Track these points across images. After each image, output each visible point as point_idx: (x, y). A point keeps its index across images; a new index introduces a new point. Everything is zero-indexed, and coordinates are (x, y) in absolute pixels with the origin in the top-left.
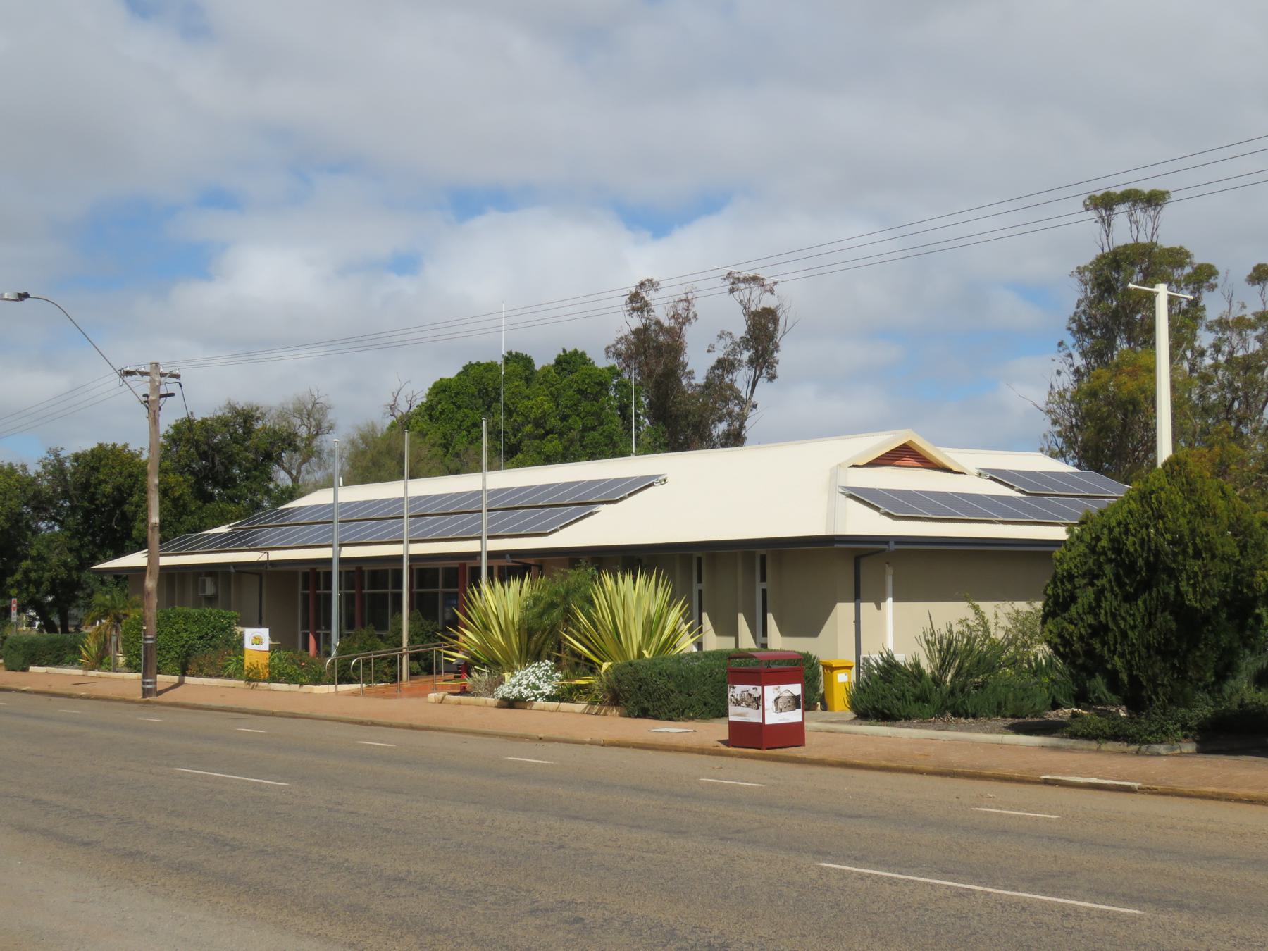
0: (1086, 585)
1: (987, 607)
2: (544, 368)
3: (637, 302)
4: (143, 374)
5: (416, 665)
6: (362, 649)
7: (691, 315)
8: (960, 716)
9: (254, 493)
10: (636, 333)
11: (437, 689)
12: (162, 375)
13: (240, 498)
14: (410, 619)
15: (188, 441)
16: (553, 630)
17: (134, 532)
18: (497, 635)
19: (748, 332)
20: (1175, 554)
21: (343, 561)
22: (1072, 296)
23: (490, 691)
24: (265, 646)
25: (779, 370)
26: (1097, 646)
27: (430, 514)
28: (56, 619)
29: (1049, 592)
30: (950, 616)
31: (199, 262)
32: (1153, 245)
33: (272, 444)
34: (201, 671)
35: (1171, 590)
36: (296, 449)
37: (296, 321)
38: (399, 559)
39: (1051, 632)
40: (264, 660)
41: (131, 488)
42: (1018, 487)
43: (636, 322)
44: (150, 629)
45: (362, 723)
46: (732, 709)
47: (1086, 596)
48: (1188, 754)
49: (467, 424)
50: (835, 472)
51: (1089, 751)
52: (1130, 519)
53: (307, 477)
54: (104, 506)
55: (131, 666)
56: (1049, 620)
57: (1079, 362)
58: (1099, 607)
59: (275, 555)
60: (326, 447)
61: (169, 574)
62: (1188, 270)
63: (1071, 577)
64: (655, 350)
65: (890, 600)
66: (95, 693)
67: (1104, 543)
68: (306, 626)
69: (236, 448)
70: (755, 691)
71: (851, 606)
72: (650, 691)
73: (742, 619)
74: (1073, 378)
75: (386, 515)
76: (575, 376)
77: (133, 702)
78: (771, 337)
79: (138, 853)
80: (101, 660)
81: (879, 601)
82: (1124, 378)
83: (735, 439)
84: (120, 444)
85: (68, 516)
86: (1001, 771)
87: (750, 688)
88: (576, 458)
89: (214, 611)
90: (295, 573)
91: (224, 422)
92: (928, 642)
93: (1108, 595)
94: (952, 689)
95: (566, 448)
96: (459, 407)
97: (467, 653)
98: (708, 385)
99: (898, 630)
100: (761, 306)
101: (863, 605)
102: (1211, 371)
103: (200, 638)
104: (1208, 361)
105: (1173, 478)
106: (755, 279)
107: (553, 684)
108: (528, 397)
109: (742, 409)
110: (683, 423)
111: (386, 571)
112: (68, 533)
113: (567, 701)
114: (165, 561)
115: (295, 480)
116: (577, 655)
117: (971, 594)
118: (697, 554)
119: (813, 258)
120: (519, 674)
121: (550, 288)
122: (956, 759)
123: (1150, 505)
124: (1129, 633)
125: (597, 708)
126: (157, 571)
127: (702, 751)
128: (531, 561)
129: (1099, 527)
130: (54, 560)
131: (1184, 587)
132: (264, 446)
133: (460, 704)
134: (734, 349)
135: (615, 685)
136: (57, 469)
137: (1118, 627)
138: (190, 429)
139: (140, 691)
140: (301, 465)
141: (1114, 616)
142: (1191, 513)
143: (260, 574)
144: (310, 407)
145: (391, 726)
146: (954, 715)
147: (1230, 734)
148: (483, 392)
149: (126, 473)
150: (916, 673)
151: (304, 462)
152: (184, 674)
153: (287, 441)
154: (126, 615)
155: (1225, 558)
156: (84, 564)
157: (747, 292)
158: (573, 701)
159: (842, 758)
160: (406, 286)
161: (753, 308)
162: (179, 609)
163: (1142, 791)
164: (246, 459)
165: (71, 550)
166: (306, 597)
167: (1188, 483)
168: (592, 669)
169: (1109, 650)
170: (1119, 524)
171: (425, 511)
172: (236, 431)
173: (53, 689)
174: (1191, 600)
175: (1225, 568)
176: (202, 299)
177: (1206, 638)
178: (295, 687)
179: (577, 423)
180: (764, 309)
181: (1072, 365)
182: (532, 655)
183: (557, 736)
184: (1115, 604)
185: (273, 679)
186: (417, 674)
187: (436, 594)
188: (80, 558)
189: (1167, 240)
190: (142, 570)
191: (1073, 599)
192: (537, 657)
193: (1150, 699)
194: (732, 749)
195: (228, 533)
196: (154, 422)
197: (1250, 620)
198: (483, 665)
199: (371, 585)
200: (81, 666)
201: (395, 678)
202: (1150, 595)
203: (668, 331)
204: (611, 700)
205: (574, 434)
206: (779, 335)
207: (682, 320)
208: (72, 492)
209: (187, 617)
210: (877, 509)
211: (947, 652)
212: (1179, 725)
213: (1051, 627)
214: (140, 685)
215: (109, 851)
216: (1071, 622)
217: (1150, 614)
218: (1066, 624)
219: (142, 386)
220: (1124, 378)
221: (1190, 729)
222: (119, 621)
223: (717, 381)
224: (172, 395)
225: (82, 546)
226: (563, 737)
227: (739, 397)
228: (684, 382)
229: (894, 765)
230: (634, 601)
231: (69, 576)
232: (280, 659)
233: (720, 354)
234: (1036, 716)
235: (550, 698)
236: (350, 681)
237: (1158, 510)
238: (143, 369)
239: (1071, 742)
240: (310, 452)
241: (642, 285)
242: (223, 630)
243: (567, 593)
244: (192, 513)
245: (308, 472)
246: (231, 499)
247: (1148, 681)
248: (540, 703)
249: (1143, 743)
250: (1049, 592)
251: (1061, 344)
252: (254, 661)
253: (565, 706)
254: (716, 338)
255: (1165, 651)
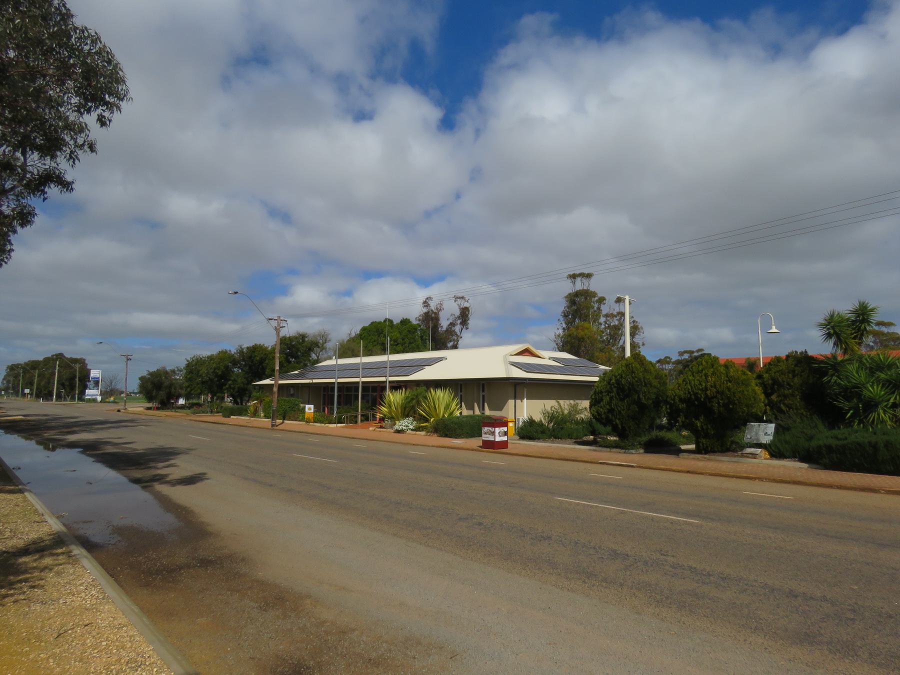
1: (561, 402)
3: (426, 304)
16: (413, 407)
23: (391, 427)
24: (312, 411)
28: (239, 400)
30: (550, 404)
31: (284, 291)
35: (636, 397)
38: (358, 383)
43: (425, 310)
44: (275, 405)
47: (606, 399)
50: (505, 357)
55: (266, 417)
57: (564, 326)
63: (601, 392)
64: (431, 318)
68: (324, 404)
72: (447, 428)
75: (354, 368)
80: (255, 414)
83: (455, 347)
91: (296, 338)
94: (556, 429)
99: (528, 409)
104: (603, 326)
106: (463, 298)
114: (280, 382)
116: (421, 415)
117: (557, 397)
119: (480, 294)
121: (397, 300)
122: (563, 454)
127: (472, 450)
131: (641, 396)
136: (241, 352)
150: (540, 424)
152: (284, 419)
153: (316, 344)
155: (655, 387)
156: (249, 383)
160: (348, 299)
168: (427, 421)
174: (644, 401)
176: (285, 302)
179: (407, 341)
182: (406, 415)
189: (592, 289)
190: (272, 385)
191: (602, 400)
192: (407, 416)
196: (278, 335)
199: (348, 392)
201: (356, 422)
203: (435, 313)
207: (439, 309)
211: (552, 417)
219: (275, 324)
230: (442, 397)
233: (451, 321)
240: (323, 348)
248: (409, 431)
253: (418, 433)
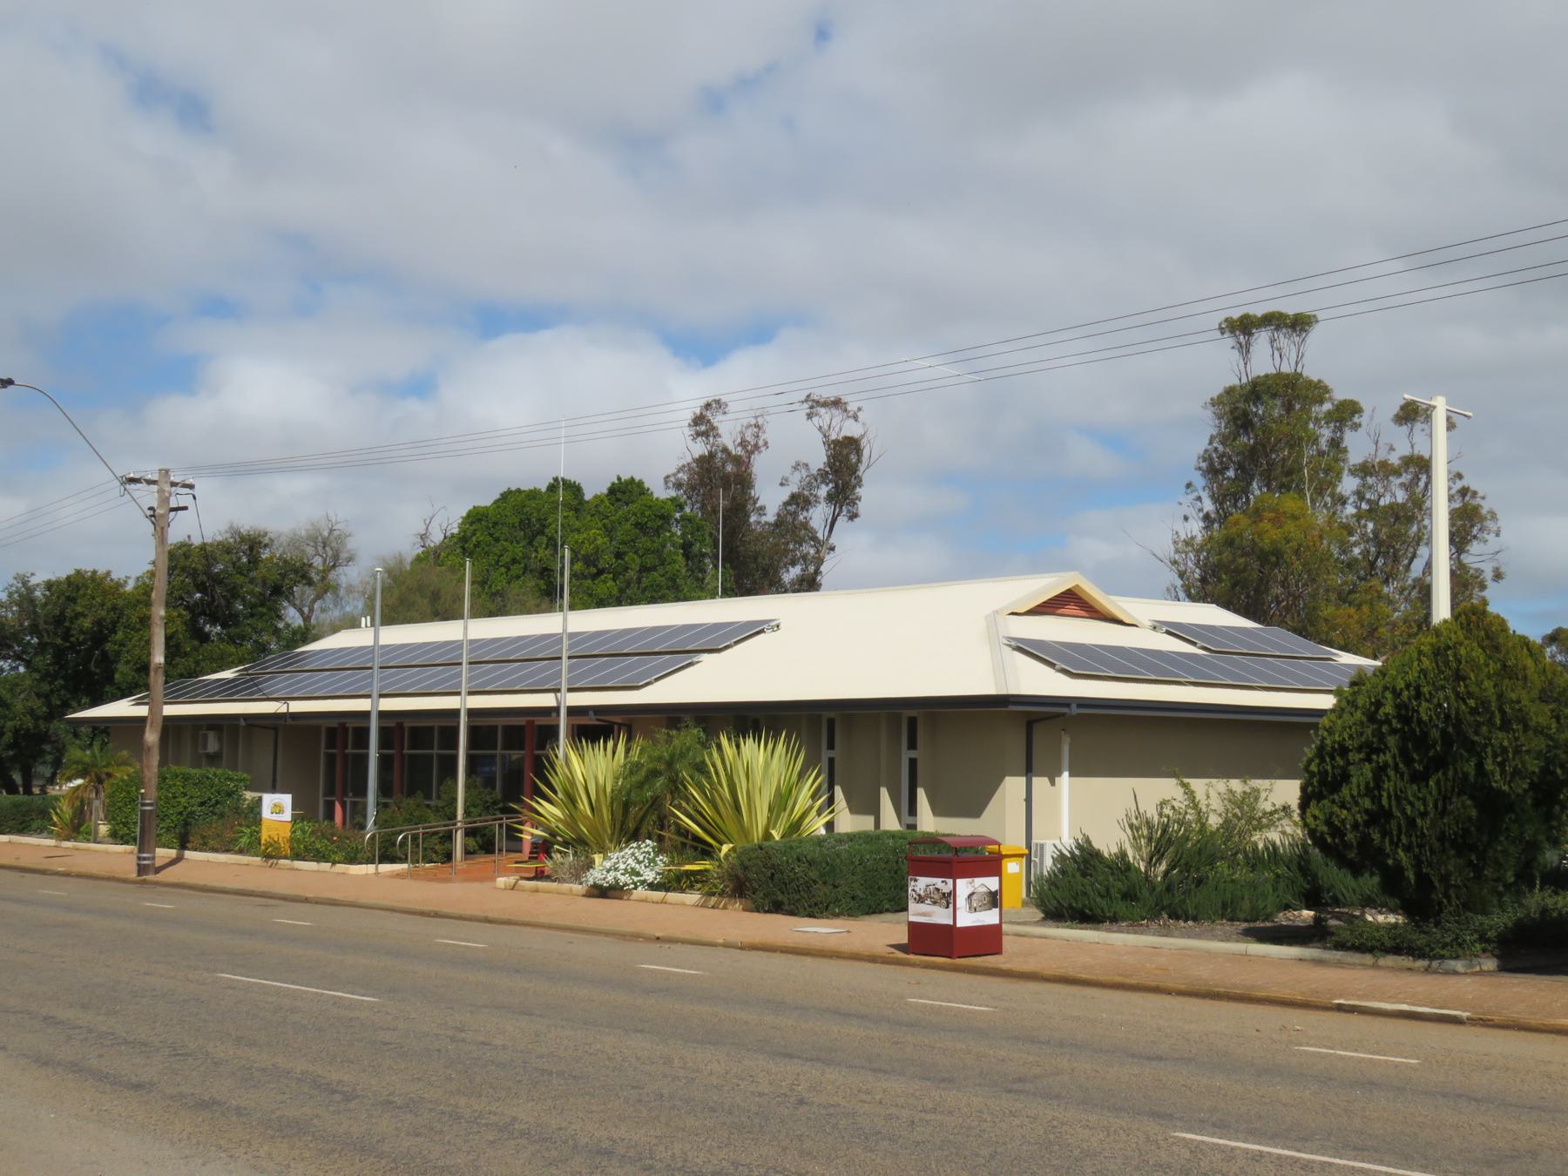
0: (1361, 760)
1: (1198, 785)
2: (596, 497)
3: (702, 424)
4: (150, 482)
5: (472, 842)
6: (408, 821)
7: (761, 443)
8: (1177, 918)
9: (259, 632)
10: (701, 460)
11: (506, 872)
12: (173, 484)
13: (243, 638)
14: (468, 787)
15: (183, 569)
16: (656, 803)
17: (117, 676)
18: (584, 806)
19: (829, 464)
20: (1479, 725)
21: (383, 715)
22: (1198, 433)
24: (287, 816)
25: (862, 507)
26: (1376, 836)
27: (496, 661)
29: (1314, 768)
30: (1155, 794)
32: (1298, 375)
33: (283, 576)
34: (205, 844)
35: (1470, 767)
36: (310, 583)
37: (294, 436)
38: (455, 713)
39: (1315, 818)
40: (286, 833)
41: (114, 623)
42: (1200, 643)
43: (700, 448)
44: (150, 793)
45: (422, 914)
46: (912, 906)
47: (1362, 774)
48: (1489, 973)
49: (506, 559)
50: (992, 619)
51: (1364, 966)
52: (1422, 681)
53: (322, 616)
54: (80, 644)
55: (116, 837)
56: (1313, 803)
57: (1208, 506)
58: (1379, 787)
59: (297, 707)
60: (343, 581)
61: (173, 726)
62: (1327, 406)
63: (1343, 750)
64: (720, 478)
65: (1066, 774)
66: (75, 869)
67: (1388, 709)
68: (330, 791)
69: (240, 580)
70: (944, 884)
71: (1021, 781)
72: (780, 880)
73: (884, 792)
74: (1201, 524)
76: (633, 507)
77: (125, 881)
78: (853, 470)
79: (215, 1102)
80: (77, 827)
81: (1053, 776)
82: (1266, 525)
83: (809, 583)
84: (101, 571)
85: (36, 654)
86: (1275, 992)
87: (938, 881)
88: (633, 601)
89: (219, 772)
90: (318, 728)
91: (226, 549)
92: (1131, 826)
93: (1391, 773)
94: (1178, 883)
95: (622, 591)
96: (497, 540)
97: (547, 829)
98: (779, 523)
99: (1076, 812)
100: (843, 434)
101: (1035, 779)
102: (1353, 522)
103: (202, 804)
104: (1350, 510)
105: (1470, 631)
106: (837, 403)
107: (657, 869)
108: (578, 530)
109: (818, 552)
110: (753, 566)
111: (431, 729)
112: (36, 676)
113: (674, 890)
114: (170, 710)
115: (307, 619)
117: (1182, 769)
118: (827, 715)
120: (615, 856)
123: (1447, 663)
124: (1419, 821)
125: (714, 900)
126: (160, 722)
127: (873, 959)
128: (617, 719)
129: (1380, 688)
130: (19, 707)
131: (1489, 765)
132: (274, 577)
133: (537, 891)
134: (810, 483)
135: (740, 873)
137: (1404, 812)
138: (186, 556)
139: (135, 868)
140: (314, 601)
141: (1398, 798)
142: (1497, 674)
143: (275, 729)
144: (326, 533)
145: (460, 918)
146: (1170, 917)
147: (1537, 948)
148: (525, 524)
149: (109, 605)
150: (1121, 866)
151: (318, 597)
154: (109, 775)
155: (1540, 731)
156: (56, 712)
157: (827, 418)
158: (682, 891)
159: (1061, 972)
161: (833, 437)
162: (174, 768)
163: (1472, 1022)
164: (251, 593)
165: (38, 695)
166: (331, 759)
167: (1488, 637)
168: (706, 852)
169: (1391, 841)
170: (1408, 686)
171: (491, 658)
172: (239, 559)
173: (23, 863)
174: (1498, 782)
175: (1540, 744)
177: (1507, 829)
178: (326, 866)
180: (846, 438)
181: (1201, 510)
182: (629, 833)
183: (679, 934)
184: (1400, 784)
185: (297, 856)
186: (474, 853)
187: (439, 756)
188: (49, 705)
189: (1311, 372)
190: (141, 720)
191: (1345, 777)
192: (635, 836)
193: (1440, 903)
194: (912, 957)
195: (234, 680)
197: (1557, 808)
198: (566, 844)
199: (417, 747)
200: (51, 834)
201: (448, 857)
202: (1445, 774)
203: (737, 460)
204: (734, 891)
205: (631, 574)
206: (862, 467)
207: (751, 448)
208: (42, 626)
209: (186, 778)
210: (1052, 665)
211: (1161, 840)
212: (1476, 936)
213: (1317, 813)
214: (133, 859)
215: (172, 1097)
216: (1343, 806)
217: (1445, 798)
218: (1336, 809)
219: (147, 496)
220: (1266, 525)
221: (1488, 941)
222: (100, 781)
223: (789, 519)
224: (185, 508)
225: (52, 691)
226: (688, 937)
227: (814, 538)
228: (753, 519)
229: (1133, 981)
231: (36, 726)
232: (304, 832)
233: (793, 488)
234: (1266, 919)
235: (652, 886)
236: (393, 860)
237: (1458, 669)
238: (149, 477)
239: (1339, 955)
241: (708, 406)
242: (229, 794)
243: (672, 756)
244: (186, 654)
245: (323, 610)
246: (232, 640)
247: (1440, 881)
248: (641, 892)
249: (1432, 958)
250: (1314, 768)
251: (1189, 485)
252: (273, 834)
253: (673, 896)
254: (790, 470)
255: (1462, 844)
